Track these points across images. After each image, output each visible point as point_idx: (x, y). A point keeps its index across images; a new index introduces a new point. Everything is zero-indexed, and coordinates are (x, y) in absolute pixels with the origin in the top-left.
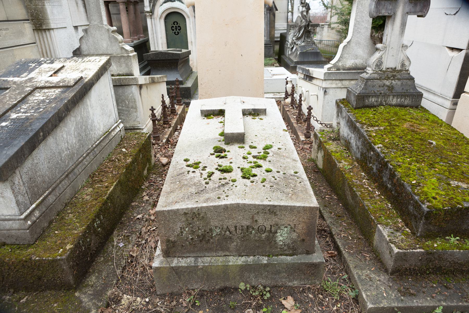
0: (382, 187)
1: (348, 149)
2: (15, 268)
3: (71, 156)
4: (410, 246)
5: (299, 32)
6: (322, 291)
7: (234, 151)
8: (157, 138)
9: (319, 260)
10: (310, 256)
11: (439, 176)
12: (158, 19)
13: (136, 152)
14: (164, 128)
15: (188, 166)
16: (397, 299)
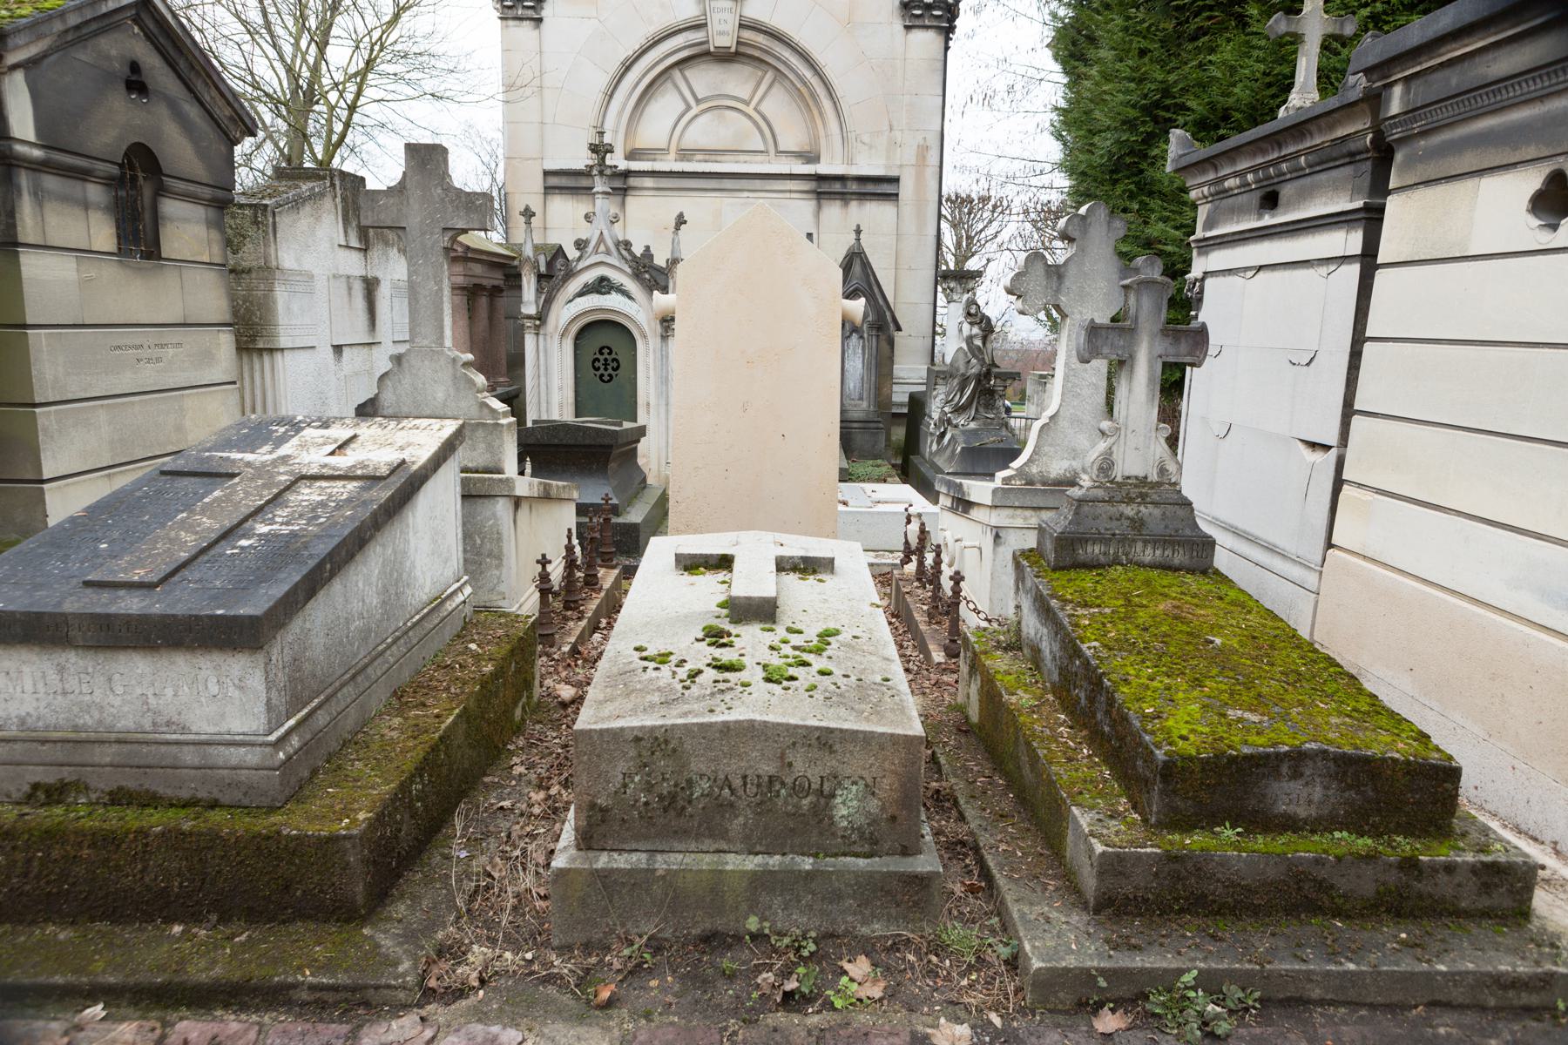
0: (1096, 738)
1: (1038, 668)
2: (238, 854)
3: (365, 633)
4: (1131, 843)
5: (962, 390)
6: (939, 948)
7: (751, 641)
8: (548, 640)
9: (929, 869)
10: (910, 859)
11: (1206, 701)
12: (557, 337)
13: (503, 652)
14: (566, 619)
15: (645, 659)
16: (1100, 955)
